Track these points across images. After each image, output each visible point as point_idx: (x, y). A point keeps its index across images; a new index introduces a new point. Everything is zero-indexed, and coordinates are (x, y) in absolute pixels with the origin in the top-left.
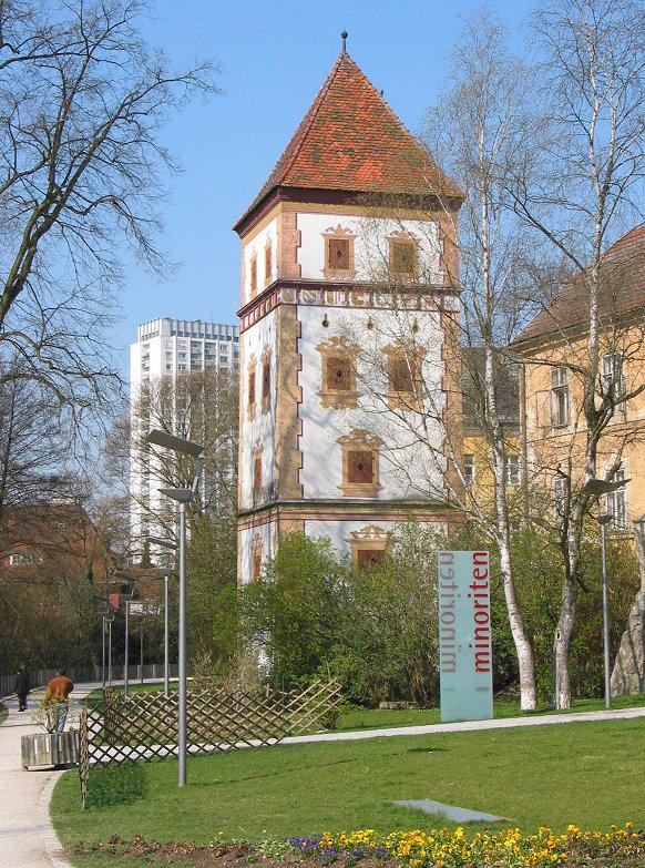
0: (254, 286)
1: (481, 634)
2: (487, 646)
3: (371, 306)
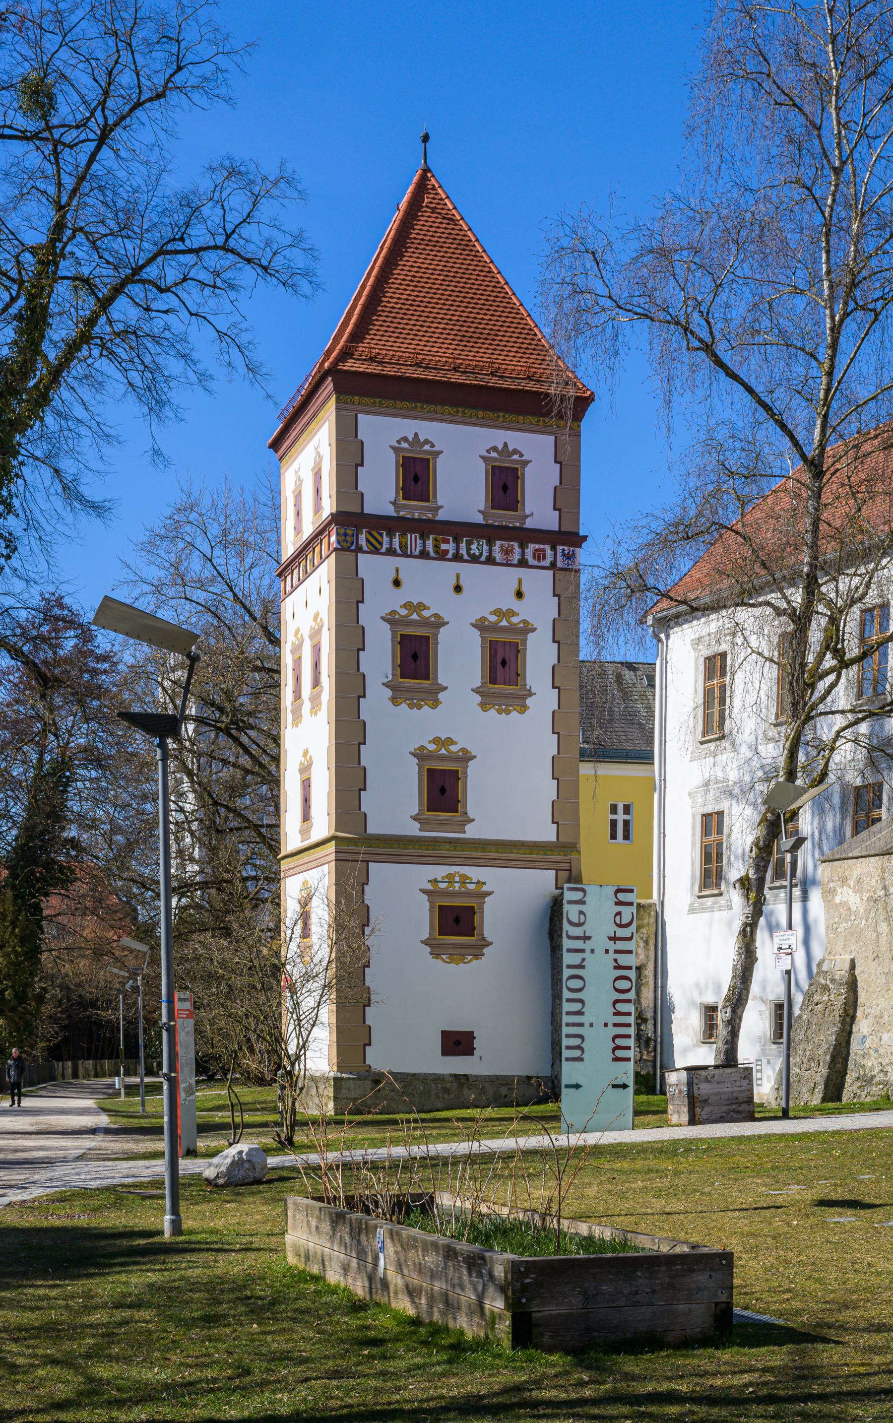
0: (298, 529)
1: (621, 1007)
2: (629, 1025)
3: (457, 558)
